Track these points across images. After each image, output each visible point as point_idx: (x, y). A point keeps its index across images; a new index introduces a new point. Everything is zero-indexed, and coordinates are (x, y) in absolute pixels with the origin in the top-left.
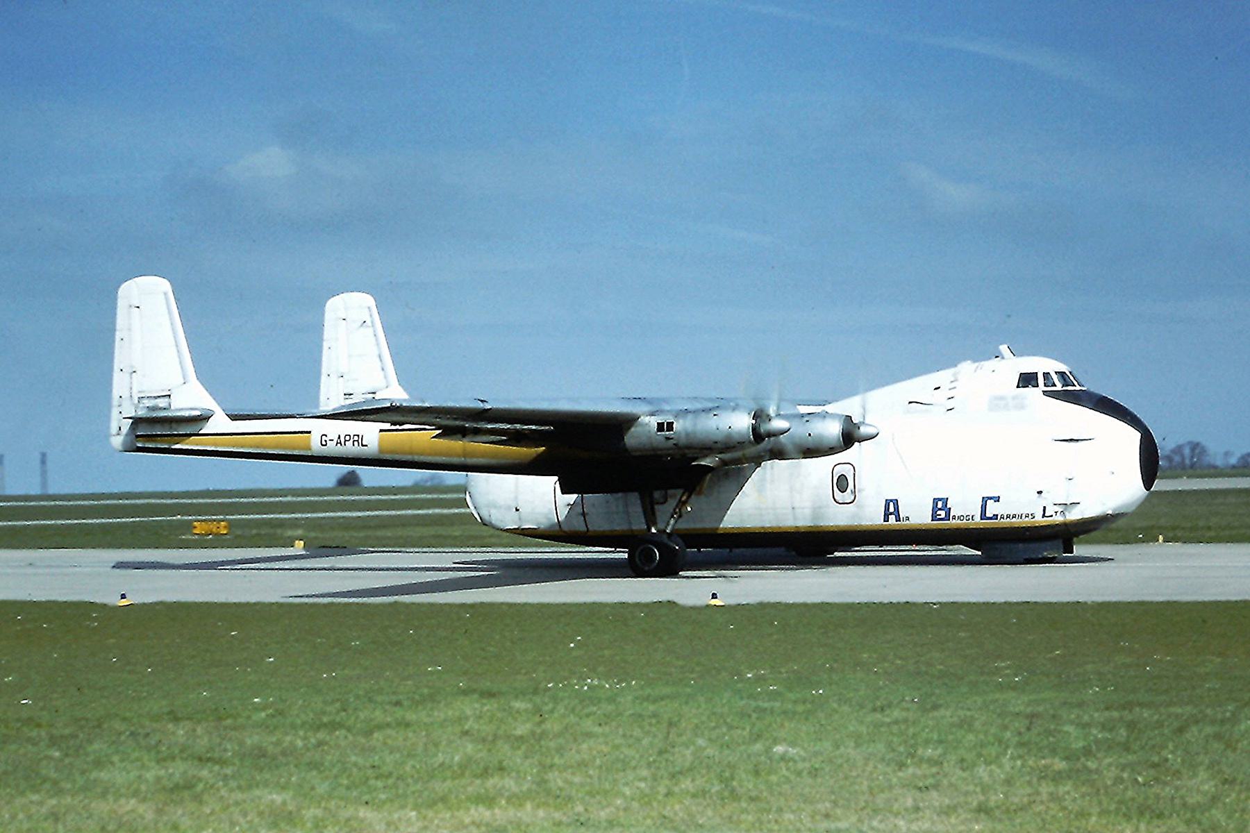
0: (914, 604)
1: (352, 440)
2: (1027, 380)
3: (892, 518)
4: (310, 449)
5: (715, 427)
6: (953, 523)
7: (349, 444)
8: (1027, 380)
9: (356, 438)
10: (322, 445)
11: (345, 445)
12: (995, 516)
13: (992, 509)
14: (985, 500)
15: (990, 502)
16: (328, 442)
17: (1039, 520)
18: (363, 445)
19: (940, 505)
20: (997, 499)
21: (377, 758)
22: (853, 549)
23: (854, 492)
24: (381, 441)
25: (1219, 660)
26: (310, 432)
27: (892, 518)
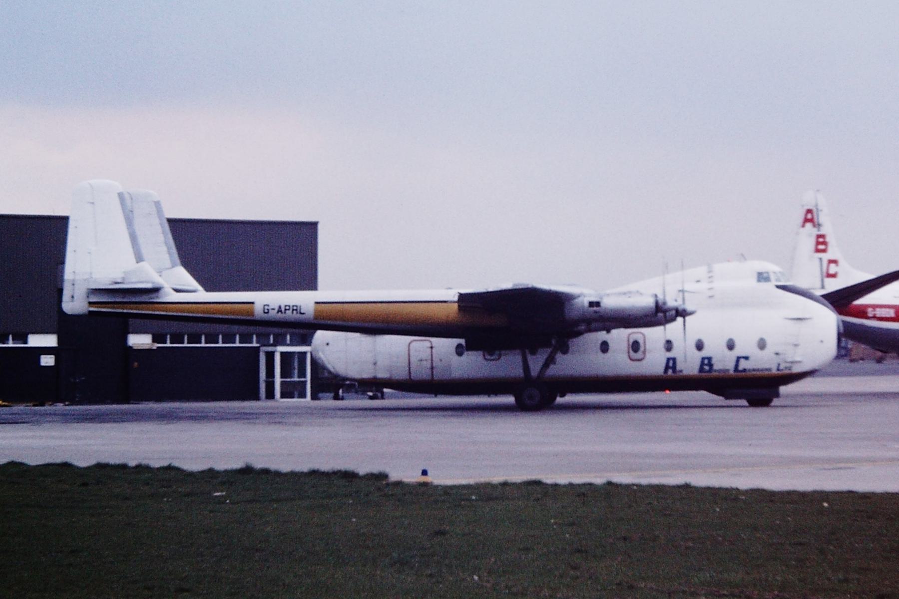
0: (278, 474)
1: (291, 310)
2: (762, 277)
3: (670, 372)
4: (253, 316)
5: (586, 304)
6: (714, 374)
7: (289, 313)
8: (762, 277)
9: (295, 308)
10: (265, 313)
11: (285, 313)
12: (744, 370)
13: (743, 365)
14: (738, 359)
15: (742, 361)
16: (270, 311)
17: (774, 371)
18: (301, 313)
19: (706, 362)
20: (746, 358)
21: (603, 504)
22: (559, 400)
23: (644, 352)
24: (316, 311)
25: (178, 582)
26: (253, 303)
27: (670, 372)
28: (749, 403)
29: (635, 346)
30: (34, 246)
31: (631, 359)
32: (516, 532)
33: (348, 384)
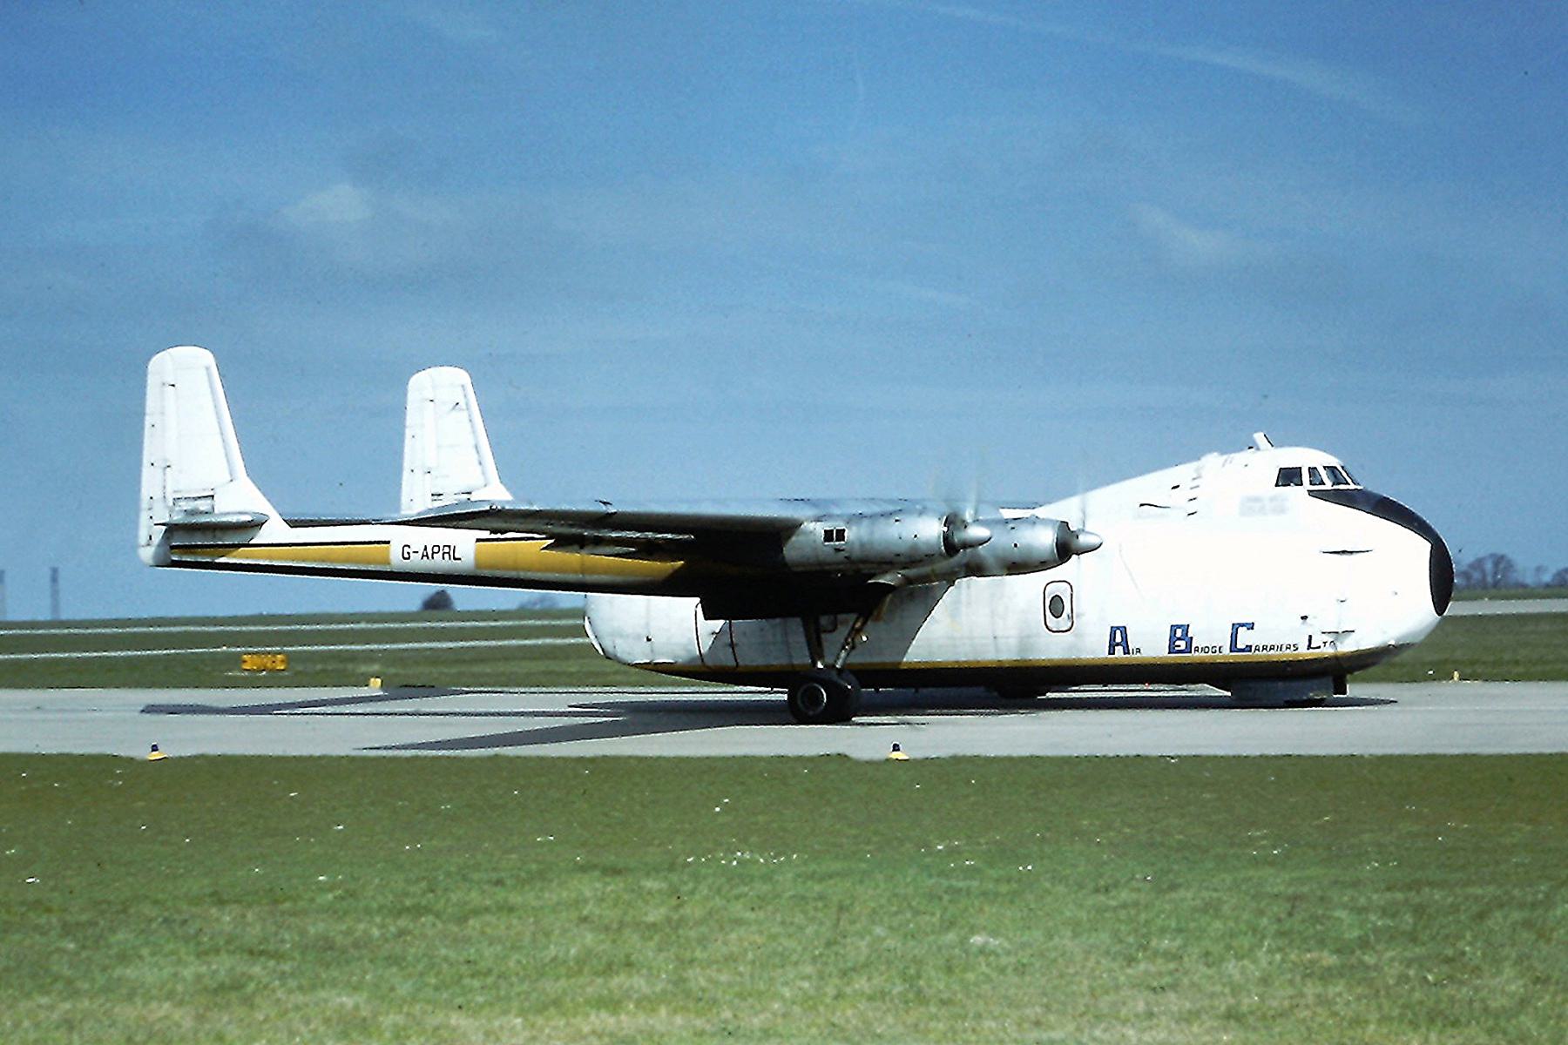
1: (441, 552)
2: (1288, 477)
3: (1119, 650)
4: (389, 564)
5: (897, 536)
6: (1196, 656)
7: (438, 557)
8: (1288, 477)
9: (447, 550)
10: (404, 558)
11: (433, 558)
12: (1249, 648)
13: (1244, 638)
14: (1236, 627)
15: (1241, 630)
16: (412, 554)
17: (1303, 652)
19: (1179, 633)
20: (1251, 626)
23: (1071, 617)
24: (477, 553)
26: (388, 542)
27: (1119, 650)
28: (913, 687)
29: (1055, 606)
30: (873, 905)
31: (1047, 627)
32: (752, 879)
33: (1466, 828)
